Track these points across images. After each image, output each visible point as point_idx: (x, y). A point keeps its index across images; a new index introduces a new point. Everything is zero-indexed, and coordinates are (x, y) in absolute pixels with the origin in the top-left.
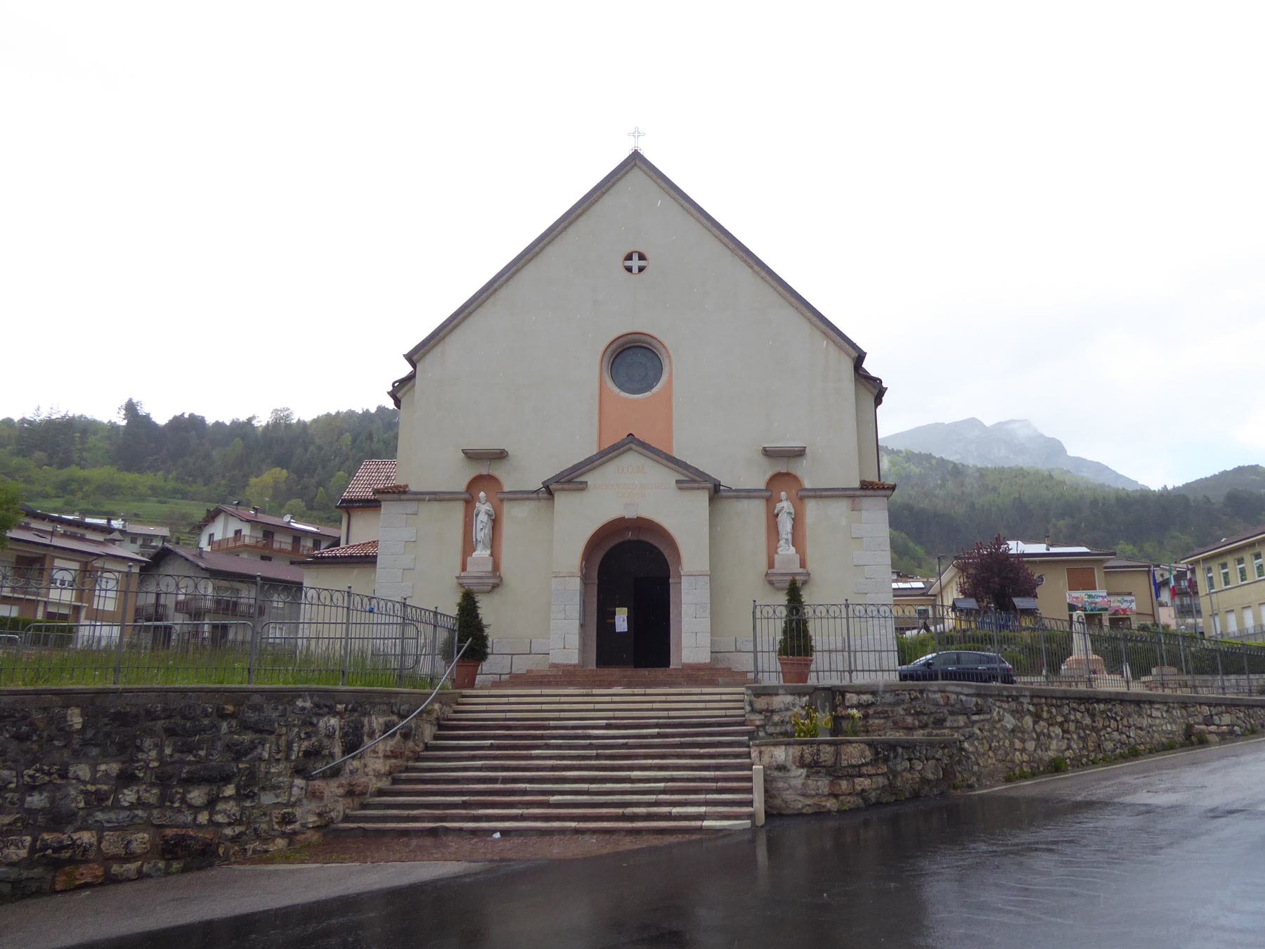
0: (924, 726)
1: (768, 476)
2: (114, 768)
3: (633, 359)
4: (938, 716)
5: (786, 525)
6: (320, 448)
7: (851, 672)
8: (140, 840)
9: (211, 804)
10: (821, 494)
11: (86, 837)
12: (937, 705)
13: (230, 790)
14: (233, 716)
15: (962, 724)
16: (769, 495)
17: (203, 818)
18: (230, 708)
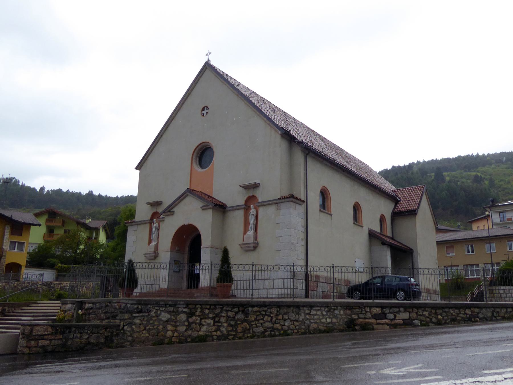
0: (108, 318)
3: (203, 154)
4: (115, 314)
5: (252, 220)
6: (412, 173)
12: (115, 309)
16: (246, 207)
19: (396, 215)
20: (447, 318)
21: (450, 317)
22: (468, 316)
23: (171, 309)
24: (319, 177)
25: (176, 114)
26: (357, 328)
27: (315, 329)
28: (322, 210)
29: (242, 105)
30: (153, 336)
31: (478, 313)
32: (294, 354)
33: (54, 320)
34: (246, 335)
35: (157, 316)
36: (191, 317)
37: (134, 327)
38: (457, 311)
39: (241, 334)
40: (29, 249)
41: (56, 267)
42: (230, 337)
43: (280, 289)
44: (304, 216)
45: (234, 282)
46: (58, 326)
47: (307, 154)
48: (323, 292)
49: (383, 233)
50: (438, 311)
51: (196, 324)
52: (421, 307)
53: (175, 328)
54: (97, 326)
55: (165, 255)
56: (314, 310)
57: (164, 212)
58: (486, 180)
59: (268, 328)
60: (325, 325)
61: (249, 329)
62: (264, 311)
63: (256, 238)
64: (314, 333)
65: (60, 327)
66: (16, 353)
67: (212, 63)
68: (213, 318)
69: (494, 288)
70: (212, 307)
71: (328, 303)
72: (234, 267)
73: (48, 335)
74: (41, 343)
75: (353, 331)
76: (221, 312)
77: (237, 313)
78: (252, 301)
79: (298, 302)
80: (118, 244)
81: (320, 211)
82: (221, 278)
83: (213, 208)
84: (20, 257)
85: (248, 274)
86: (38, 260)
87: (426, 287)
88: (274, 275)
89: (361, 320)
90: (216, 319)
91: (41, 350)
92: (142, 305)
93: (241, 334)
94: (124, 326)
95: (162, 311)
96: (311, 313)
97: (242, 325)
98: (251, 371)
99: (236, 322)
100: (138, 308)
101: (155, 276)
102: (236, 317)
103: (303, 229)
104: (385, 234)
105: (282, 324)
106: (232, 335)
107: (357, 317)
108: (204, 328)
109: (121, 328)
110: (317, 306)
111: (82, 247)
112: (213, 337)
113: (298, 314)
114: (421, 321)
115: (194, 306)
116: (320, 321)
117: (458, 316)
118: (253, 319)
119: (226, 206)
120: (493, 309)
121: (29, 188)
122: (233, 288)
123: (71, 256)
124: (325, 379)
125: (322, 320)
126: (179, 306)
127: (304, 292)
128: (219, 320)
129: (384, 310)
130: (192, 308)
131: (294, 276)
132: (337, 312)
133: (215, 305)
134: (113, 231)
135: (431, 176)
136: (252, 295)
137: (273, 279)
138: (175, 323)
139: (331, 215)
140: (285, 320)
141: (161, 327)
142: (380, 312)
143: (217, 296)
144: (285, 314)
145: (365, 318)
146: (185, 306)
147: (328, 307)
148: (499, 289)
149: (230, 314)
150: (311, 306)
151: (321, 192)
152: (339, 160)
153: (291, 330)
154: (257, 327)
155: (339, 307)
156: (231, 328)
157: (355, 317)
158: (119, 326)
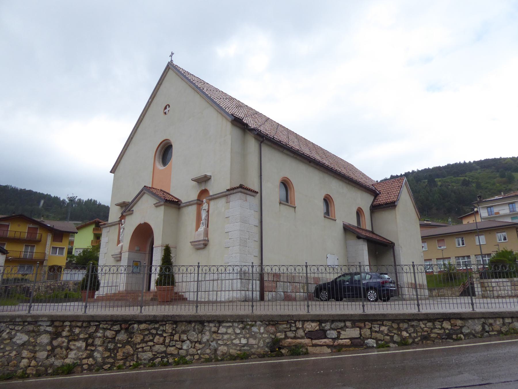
1: (198, 193)
3: (165, 151)
16: (199, 202)
19: (375, 208)
20: (415, 335)
21: (419, 334)
22: (447, 331)
23: (31, 328)
24: (277, 166)
25: (144, 117)
26: (283, 351)
27: (224, 354)
31: (461, 327)
34: (128, 364)
35: (11, 339)
36: (56, 338)
38: (429, 324)
42: (106, 367)
45: (177, 284)
47: (262, 142)
48: (284, 292)
49: (361, 227)
50: (401, 325)
51: (61, 348)
52: (376, 320)
53: (33, 355)
56: (224, 327)
58: (473, 183)
59: (158, 353)
60: (238, 348)
61: (133, 355)
62: (154, 328)
67: (175, 63)
68: (85, 340)
69: (485, 281)
70: (84, 325)
76: (96, 331)
77: (118, 332)
82: (161, 281)
83: (164, 205)
84: (61, 260)
87: (410, 281)
89: (289, 340)
93: (121, 362)
95: (18, 331)
96: (219, 332)
97: (124, 350)
102: (117, 338)
104: (364, 228)
105: (179, 346)
106: (108, 363)
107: (283, 337)
110: (228, 322)
112: (82, 367)
113: (201, 332)
114: (377, 340)
115: (61, 324)
117: (432, 333)
118: (139, 340)
119: (181, 202)
120: (483, 320)
126: (40, 323)
128: (93, 342)
129: (323, 325)
131: (243, 275)
132: (255, 329)
135: (424, 182)
138: (32, 347)
140: (183, 341)
141: (14, 353)
142: (318, 328)
144: (184, 332)
145: (295, 338)
147: (242, 322)
148: (491, 282)
149: (109, 334)
153: (191, 355)
154: (144, 351)
155: (258, 323)
157: (280, 336)
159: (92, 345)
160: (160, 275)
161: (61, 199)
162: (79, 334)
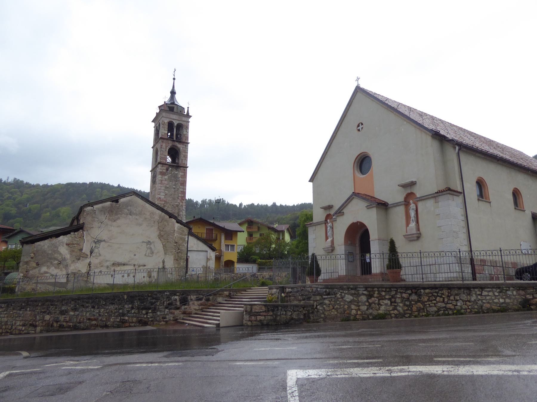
0: (304, 300)
1: (404, 195)
2: (130, 306)
3: (363, 163)
4: (309, 296)
5: (412, 214)
7: (422, 274)
8: (135, 319)
9: (147, 313)
10: (423, 199)
11: (126, 318)
12: (309, 292)
13: (150, 311)
14: (150, 296)
15: (318, 299)
16: (406, 203)
17: (145, 316)
18: (150, 295)
23: (353, 292)
24: (473, 169)
25: (336, 134)
26: (532, 307)
27: (488, 309)
28: (480, 199)
29: (392, 116)
30: (340, 313)
32: (475, 331)
33: (265, 301)
34: (421, 314)
37: (325, 306)
39: (416, 313)
40: (238, 249)
41: (257, 262)
42: (407, 315)
43: (447, 272)
44: (462, 206)
46: (269, 305)
51: (375, 304)
54: (297, 306)
55: (341, 249)
57: (336, 213)
60: (498, 305)
63: (418, 229)
64: (487, 312)
65: (271, 307)
66: (242, 325)
67: (362, 86)
70: (387, 290)
71: (499, 284)
72: (400, 255)
73: (263, 312)
74: (259, 318)
75: (528, 310)
76: (396, 294)
77: (410, 294)
78: (423, 284)
79: (468, 284)
80: (300, 242)
81: (478, 200)
82: (390, 266)
83: (376, 207)
84: (232, 255)
85: (414, 261)
86: (245, 257)
88: (440, 260)
90: (393, 300)
91: (259, 323)
92: (329, 288)
94: (317, 306)
95: (345, 294)
98: (438, 344)
99: (410, 302)
100: (326, 291)
101: (335, 265)
102: (410, 298)
103: (463, 218)
105: (455, 304)
106: (408, 313)
108: (383, 308)
109: (315, 307)
110: (488, 288)
111: (273, 246)
113: (469, 294)
116: (493, 302)
118: (426, 299)
121: (232, 205)
122: (401, 273)
123: (267, 253)
124: (514, 354)
125: (495, 301)
127: (470, 276)
130: (370, 291)
131: (460, 261)
132: (509, 293)
133: (390, 288)
134: (294, 232)
136: (423, 279)
137: (410, 266)
139: (490, 203)
143: (388, 280)
144: (457, 295)
146: (364, 289)
147: (499, 288)
149: (404, 295)
150: (482, 287)
151: (477, 182)
152: (492, 151)
154: (430, 307)
155: (511, 288)
156: (407, 308)
157: (529, 297)
158: (313, 306)
159: (395, 302)
160: (390, 260)
161: (200, 202)
162: (385, 296)
